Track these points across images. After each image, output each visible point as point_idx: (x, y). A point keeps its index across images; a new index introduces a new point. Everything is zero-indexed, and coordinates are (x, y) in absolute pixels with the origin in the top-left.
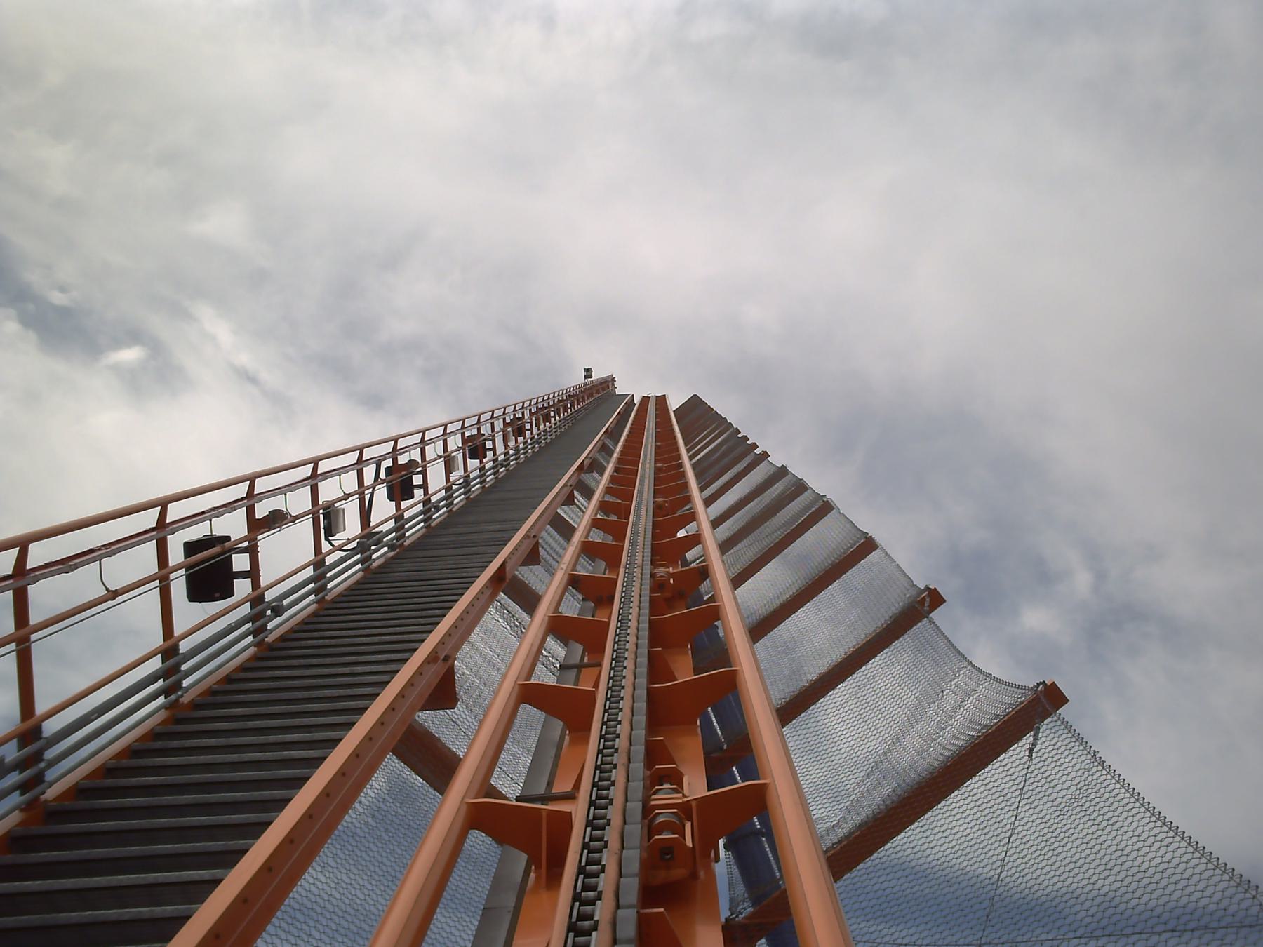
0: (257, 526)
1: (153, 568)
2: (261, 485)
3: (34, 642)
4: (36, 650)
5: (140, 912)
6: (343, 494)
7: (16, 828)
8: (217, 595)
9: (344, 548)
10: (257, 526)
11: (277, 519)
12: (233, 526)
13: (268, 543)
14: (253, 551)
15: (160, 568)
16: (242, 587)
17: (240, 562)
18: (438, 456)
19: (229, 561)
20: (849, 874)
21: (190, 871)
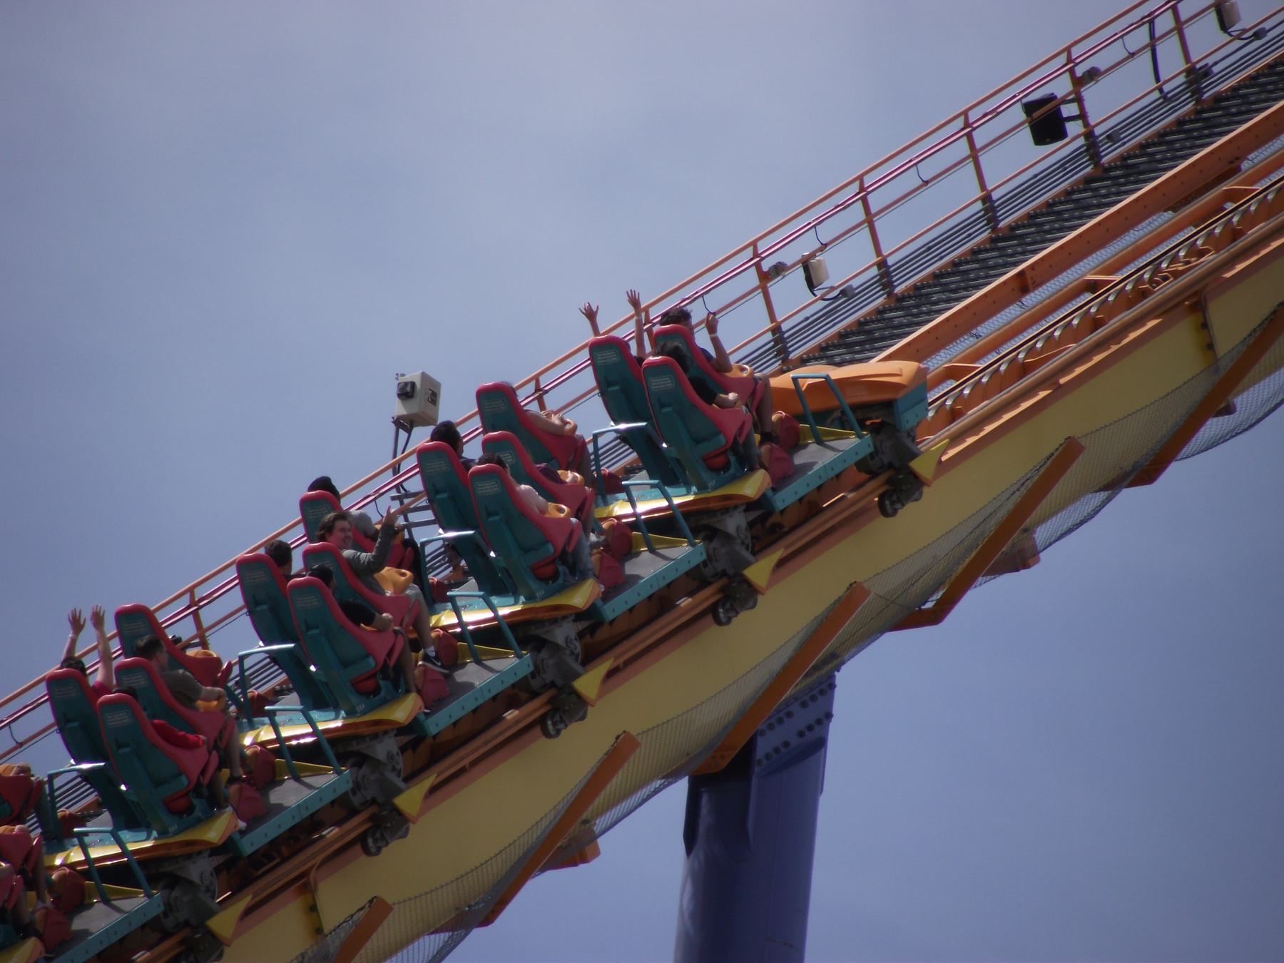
0: (1079, 82)
1: (863, 217)
2: (1076, 52)
3: (592, 390)
4: (877, 224)
5: (977, 434)
6: (820, 245)
7: (917, 327)
8: (1048, 140)
9: (1244, 36)
10: (1079, 82)
11: (779, 269)
12: (1062, 87)
13: (1090, 93)
14: (1079, 100)
15: (971, 151)
16: (1074, 128)
17: (1069, 110)
18: (1129, 53)
19: (1058, 112)
20: (938, 597)
21: (973, 408)
